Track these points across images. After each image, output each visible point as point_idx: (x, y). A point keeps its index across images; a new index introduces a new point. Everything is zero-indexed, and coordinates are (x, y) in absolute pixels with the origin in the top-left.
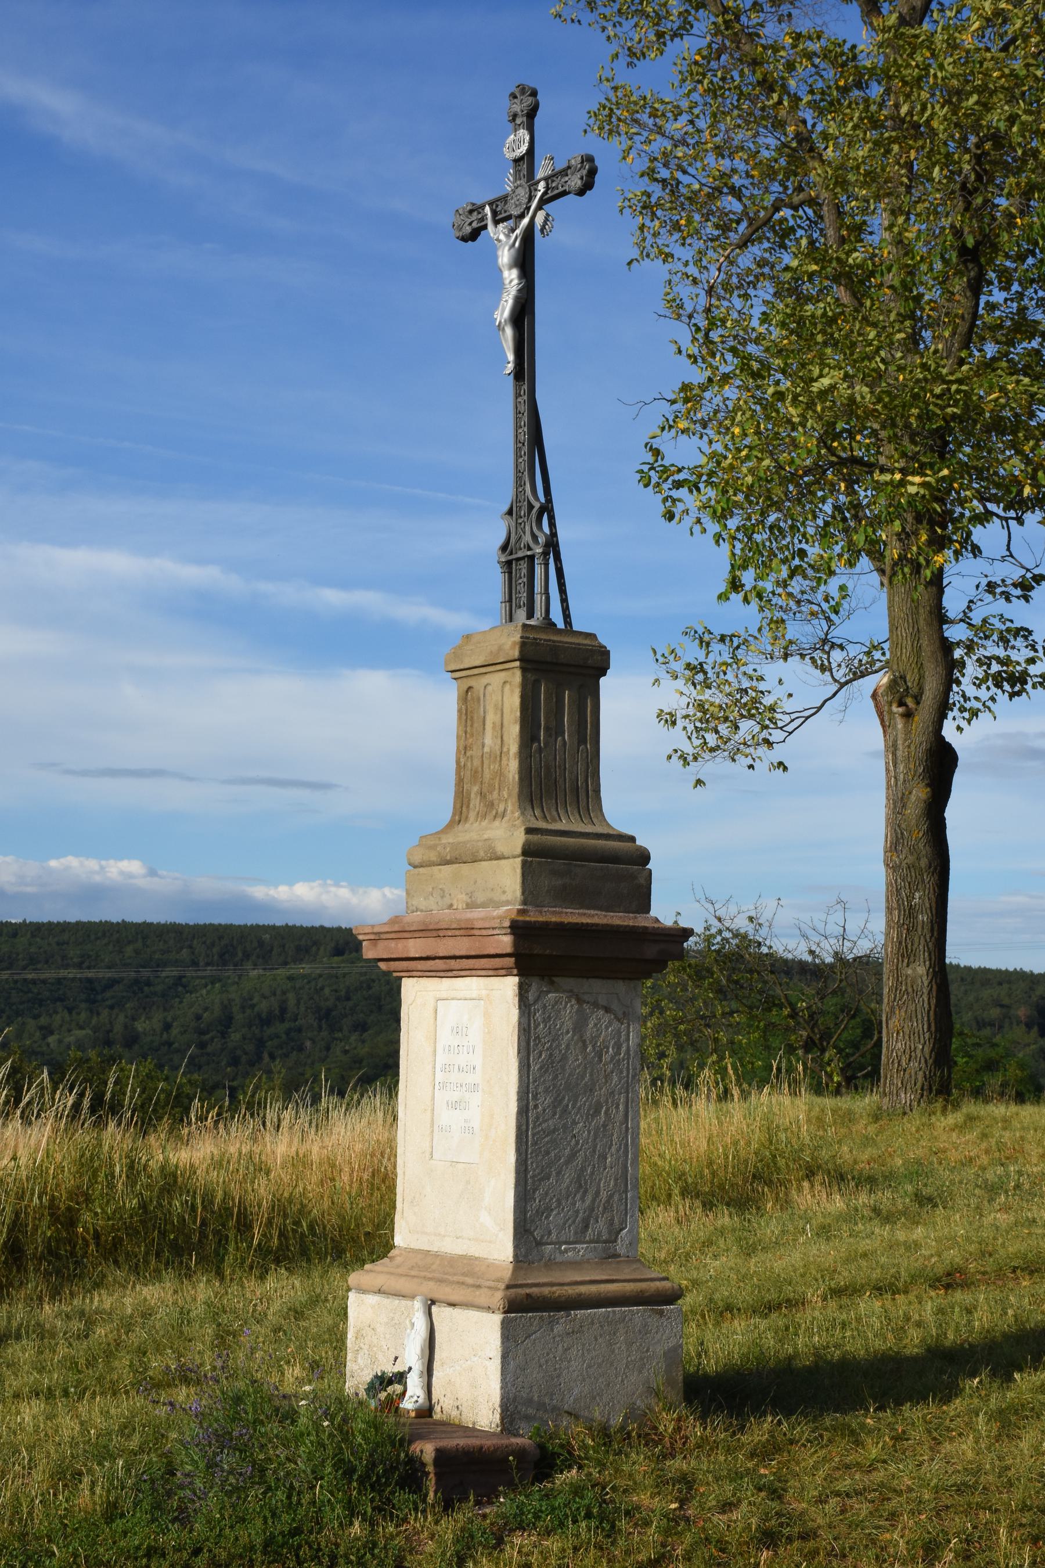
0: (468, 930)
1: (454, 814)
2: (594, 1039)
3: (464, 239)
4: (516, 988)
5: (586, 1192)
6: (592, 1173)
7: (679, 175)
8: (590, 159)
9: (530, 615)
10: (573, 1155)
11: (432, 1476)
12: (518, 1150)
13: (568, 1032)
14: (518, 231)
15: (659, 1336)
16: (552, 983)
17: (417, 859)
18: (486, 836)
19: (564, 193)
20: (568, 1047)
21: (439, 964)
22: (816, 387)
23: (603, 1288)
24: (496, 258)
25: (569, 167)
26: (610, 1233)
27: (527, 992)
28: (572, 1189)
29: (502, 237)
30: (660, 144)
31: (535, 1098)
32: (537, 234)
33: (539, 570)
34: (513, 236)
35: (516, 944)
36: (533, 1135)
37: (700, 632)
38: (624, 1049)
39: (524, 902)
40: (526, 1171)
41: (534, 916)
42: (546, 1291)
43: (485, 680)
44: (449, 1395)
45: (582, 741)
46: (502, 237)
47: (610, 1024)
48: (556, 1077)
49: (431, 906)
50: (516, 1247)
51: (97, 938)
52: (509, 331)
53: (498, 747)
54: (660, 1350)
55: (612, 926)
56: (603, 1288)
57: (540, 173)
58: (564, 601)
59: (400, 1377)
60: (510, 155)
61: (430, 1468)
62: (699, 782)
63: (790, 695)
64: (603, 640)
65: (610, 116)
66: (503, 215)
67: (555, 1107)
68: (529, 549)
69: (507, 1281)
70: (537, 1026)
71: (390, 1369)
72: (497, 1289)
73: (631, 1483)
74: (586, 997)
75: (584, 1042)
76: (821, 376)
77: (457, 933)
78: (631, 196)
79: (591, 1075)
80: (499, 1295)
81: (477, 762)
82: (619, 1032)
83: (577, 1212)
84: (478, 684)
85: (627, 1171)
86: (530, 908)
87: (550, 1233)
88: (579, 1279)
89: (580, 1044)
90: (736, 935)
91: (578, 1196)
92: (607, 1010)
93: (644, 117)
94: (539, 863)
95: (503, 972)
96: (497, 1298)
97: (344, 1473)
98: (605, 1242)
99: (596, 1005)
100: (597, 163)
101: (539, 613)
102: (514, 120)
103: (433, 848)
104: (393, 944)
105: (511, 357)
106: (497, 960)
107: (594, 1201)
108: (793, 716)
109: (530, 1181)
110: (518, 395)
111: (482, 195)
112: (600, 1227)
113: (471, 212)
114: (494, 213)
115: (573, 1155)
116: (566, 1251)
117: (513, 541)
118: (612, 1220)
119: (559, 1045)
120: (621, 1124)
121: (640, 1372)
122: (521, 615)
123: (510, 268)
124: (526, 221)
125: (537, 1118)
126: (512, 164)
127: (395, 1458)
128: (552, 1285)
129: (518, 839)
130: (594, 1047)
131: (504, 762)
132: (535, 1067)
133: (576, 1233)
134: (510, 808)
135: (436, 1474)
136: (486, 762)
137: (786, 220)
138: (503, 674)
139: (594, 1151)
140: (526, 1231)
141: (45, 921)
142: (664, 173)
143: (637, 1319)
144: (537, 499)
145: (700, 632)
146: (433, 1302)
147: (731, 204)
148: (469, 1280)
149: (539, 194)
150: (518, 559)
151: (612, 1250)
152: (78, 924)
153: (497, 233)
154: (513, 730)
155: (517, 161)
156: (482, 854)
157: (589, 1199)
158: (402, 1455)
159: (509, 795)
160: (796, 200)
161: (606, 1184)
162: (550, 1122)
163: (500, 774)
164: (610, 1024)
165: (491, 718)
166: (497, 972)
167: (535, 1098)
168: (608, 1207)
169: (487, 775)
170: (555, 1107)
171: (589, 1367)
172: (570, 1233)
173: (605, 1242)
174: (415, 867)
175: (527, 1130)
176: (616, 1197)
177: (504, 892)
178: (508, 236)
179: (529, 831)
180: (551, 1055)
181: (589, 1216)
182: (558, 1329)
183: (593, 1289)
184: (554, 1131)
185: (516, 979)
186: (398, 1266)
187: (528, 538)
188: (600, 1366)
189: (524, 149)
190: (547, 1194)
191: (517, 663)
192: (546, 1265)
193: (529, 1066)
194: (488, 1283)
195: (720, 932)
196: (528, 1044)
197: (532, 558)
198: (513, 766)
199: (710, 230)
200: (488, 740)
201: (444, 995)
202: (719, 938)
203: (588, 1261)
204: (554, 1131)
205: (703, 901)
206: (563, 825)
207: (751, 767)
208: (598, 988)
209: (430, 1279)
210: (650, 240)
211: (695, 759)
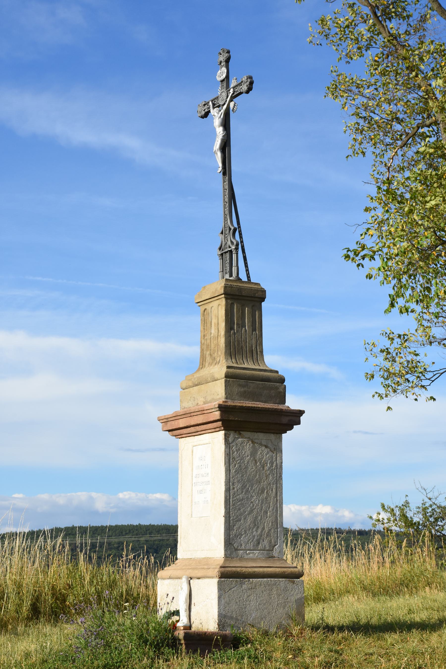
0: (202, 412)
1: (200, 365)
2: (260, 460)
3: (202, 117)
4: (223, 436)
5: (258, 527)
6: (261, 519)
7: (372, 115)
8: (251, 77)
9: (231, 275)
10: (252, 511)
11: (184, 645)
12: (226, 507)
13: (248, 456)
14: (222, 111)
15: (293, 592)
16: (240, 434)
17: (184, 386)
18: (211, 372)
19: (241, 93)
20: (248, 462)
21: (192, 429)
22: (428, 205)
23: (265, 569)
24: (213, 123)
25: (242, 82)
26: (270, 546)
27: (228, 437)
28: (252, 526)
29: (216, 114)
30: (360, 100)
31: (233, 484)
32: (231, 112)
33: (234, 256)
34: (220, 113)
35: (221, 415)
36: (233, 501)
37: (388, 333)
38: (275, 464)
39: (226, 398)
40: (229, 517)
41: (230, 403)
42: (239, 569)
43: (211, 305)
44: (197, 619)
45: (254, 329)
46: (216, 114)
47: (268, 453)
48: (243, 476)
49: (190, 405)
50: (226, 551)
51: (126, 534)
52: (219, 154)
53: (216, 333)
54: (293, 599)
55: (266, 408)
56: (265, 569)
57: (232, 85)
58: (247, 270)
59: (177, 613)
60: (219, 79)
61: (183, 642)
62: (389, 408)
63: (433, 363)
64: (263, 286)
65: (336, 88)
66: (217, 105)
67: (242, 489)
68: (230, 247)
69: (221, 565)
70: (233, 453)
71: (173, 609)
72: (215, 568)
73: (273, 649)
74: (256, 441)
75: (256, 461)
76: (431, 200)
77: (198, 413)
78: (349, 125)
79: (259, 475)
80: (217, 570)
81: (208, 341)
82: (272, 457)
83: (254, 536)
84: (208, 307)
85: (277, 519)
86: (229, 400)
87: (241, 545)
88: (255, 565)
89: (254, 462)
90: (439, 507)
91: (254, 529)
92: (266, 447)
93: (354, 89)
94: (233, 381)
95: (218, 429)
96: (216, 572)
97: (143, 642)
98: (268, 550)
99: (261, 444)
100: (253, 79)
101: (234, 274)
102: (220, 64)
103: (190, 380)
104: (173, 422)
105: (220, 165)
106: (215, 423)
107: (262, 532)
108: (435, 373)
109: (231, 521)
110: (224, 182)
111: (209, 98)
112: (265, 543)
113: (204, 105)
114: (214, 105)
115: (252, 511)
116: (249, 554)
117: (223, 245)
118: (271, 541)
119: (244, 462)
120: (274, 498)
121: (284, 608)
122: (227, 276)
123: (219, 127)
124: (225, 107)
125: (234, 494)
126: (220, 83)
127: (167, 639)
128: (242, 567)
129: (224, 370)
130: (260, 463)
131: (219, 339)
132: (233, 471)
133: (254, 546)
134: (221, 359)
135: (185, 644)
136: (212, 340)
137: (425, 133)
138: (218, 301)
139: (262, 509)
140: (230, 544)
141: (100, 525)
142: (364, 114)
143: (282, 584)
144: (233, 225)
145: (388, 333)
146: (191, 578)
147: (397, 127)
148: (206, 567)
149: (231, 94)
150: (226, 253)
151: (271, 555)
152: (116, 526)
153: (214, 112)
154: (222, 325)
155: (222, 81)
156: (209, 379)
157: (260, 530)
158: (170, 636)
159: (221, 353)
160: (428, 122)
161: (267, 524)
162: (241, 496)
163: (218, 345)
164: (268, 453)
165: (214, 321)
166: (216, 430)
167: (233, 484)
168: (268, 535)
169: (213, 346)
170: (242, 489)
171: (260, 604)
172: (251, 546)
173: (268, 550)
174: (184, 389)
175: (230, 499)
176: (272, 531)
177: (218, 395)
178: (218, 113)
179: (228, 367)
180: (240, 466)
181: (260, 539)
182: (244, 586)
183: (261, 570)
184: (242, 500)
185: (223, 432)
186: (178, 566)
187: (229, 243)
188: (265, 604)
189: (224, 76)
190: (239, 527)
191: (223, 296)
192: (240, 559)
193: (230, 470)
194: (213, 567)
195: (431, 506)
196: (229, 460)
197: (231, 251)
198: (222, 341)
199: (388, 140)
200: (213, 331)
201: (195, 444)
202: (430, 509)
203: (260, 559)
204: (242, 500)
205: (420, 489)
206: (246, 366)
207: (416, 400)
208: (261, 436)
209: (190, 569)
210: (357, 146)
211: (386, 396)
